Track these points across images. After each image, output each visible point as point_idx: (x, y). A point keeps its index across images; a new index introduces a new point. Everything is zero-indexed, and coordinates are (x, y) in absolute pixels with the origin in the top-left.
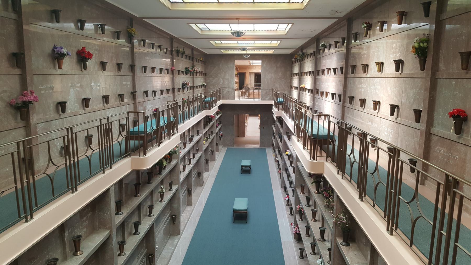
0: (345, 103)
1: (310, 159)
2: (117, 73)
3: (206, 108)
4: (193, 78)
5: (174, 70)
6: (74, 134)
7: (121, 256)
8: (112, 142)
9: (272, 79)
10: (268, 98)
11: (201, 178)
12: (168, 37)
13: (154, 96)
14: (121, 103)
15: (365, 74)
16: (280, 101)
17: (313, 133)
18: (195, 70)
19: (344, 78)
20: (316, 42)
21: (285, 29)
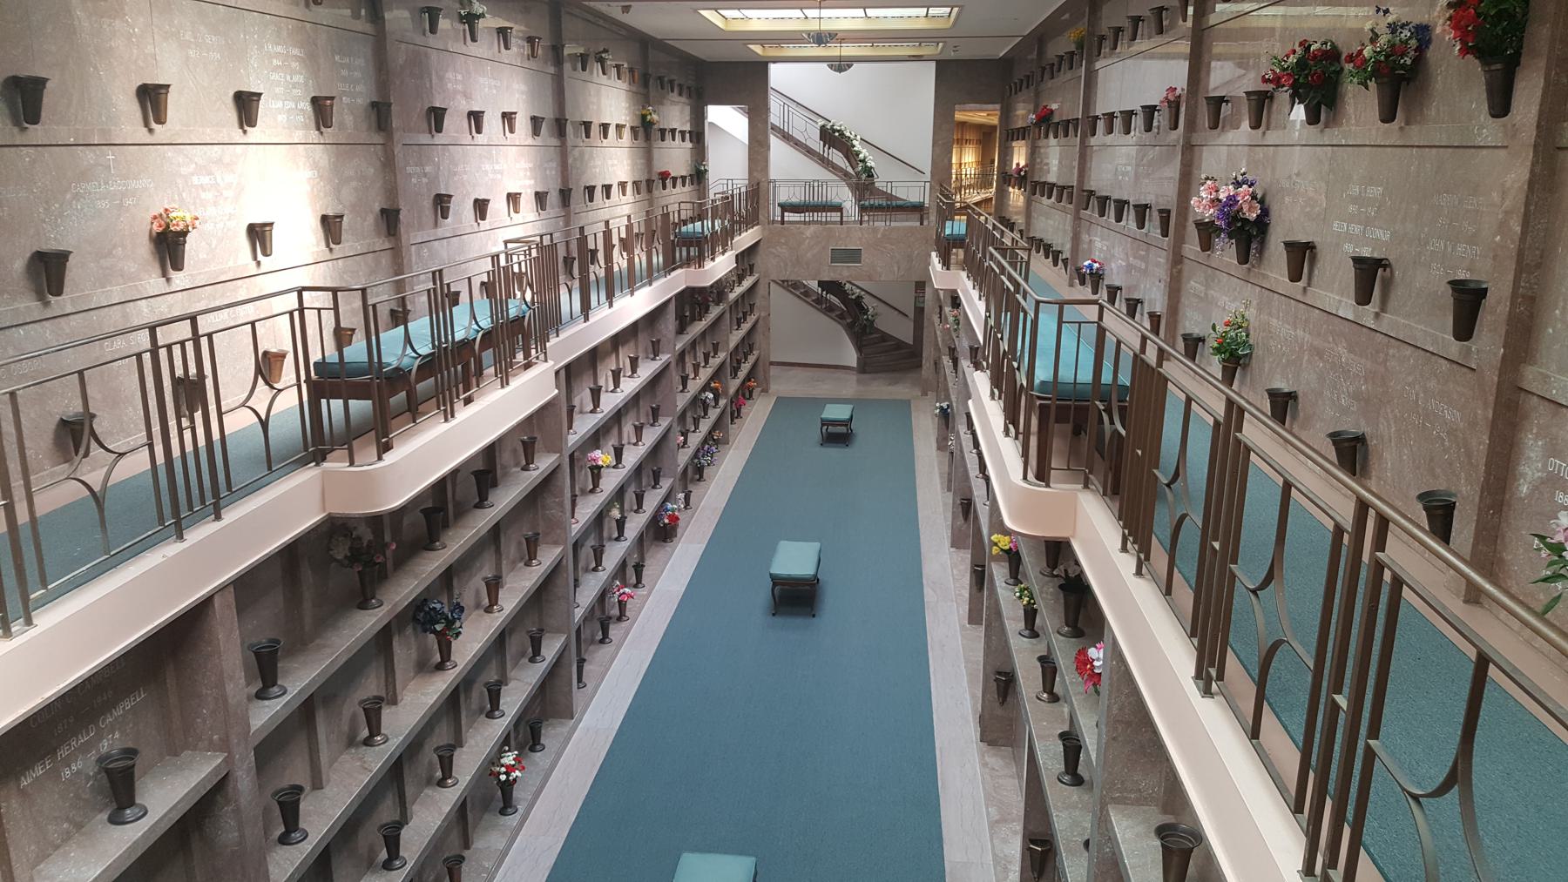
1: (1021, 477)
2: (314, 135)
3: (687, 263)
7: (493, 718)
8: (220, 414)
20: (1087, 14)
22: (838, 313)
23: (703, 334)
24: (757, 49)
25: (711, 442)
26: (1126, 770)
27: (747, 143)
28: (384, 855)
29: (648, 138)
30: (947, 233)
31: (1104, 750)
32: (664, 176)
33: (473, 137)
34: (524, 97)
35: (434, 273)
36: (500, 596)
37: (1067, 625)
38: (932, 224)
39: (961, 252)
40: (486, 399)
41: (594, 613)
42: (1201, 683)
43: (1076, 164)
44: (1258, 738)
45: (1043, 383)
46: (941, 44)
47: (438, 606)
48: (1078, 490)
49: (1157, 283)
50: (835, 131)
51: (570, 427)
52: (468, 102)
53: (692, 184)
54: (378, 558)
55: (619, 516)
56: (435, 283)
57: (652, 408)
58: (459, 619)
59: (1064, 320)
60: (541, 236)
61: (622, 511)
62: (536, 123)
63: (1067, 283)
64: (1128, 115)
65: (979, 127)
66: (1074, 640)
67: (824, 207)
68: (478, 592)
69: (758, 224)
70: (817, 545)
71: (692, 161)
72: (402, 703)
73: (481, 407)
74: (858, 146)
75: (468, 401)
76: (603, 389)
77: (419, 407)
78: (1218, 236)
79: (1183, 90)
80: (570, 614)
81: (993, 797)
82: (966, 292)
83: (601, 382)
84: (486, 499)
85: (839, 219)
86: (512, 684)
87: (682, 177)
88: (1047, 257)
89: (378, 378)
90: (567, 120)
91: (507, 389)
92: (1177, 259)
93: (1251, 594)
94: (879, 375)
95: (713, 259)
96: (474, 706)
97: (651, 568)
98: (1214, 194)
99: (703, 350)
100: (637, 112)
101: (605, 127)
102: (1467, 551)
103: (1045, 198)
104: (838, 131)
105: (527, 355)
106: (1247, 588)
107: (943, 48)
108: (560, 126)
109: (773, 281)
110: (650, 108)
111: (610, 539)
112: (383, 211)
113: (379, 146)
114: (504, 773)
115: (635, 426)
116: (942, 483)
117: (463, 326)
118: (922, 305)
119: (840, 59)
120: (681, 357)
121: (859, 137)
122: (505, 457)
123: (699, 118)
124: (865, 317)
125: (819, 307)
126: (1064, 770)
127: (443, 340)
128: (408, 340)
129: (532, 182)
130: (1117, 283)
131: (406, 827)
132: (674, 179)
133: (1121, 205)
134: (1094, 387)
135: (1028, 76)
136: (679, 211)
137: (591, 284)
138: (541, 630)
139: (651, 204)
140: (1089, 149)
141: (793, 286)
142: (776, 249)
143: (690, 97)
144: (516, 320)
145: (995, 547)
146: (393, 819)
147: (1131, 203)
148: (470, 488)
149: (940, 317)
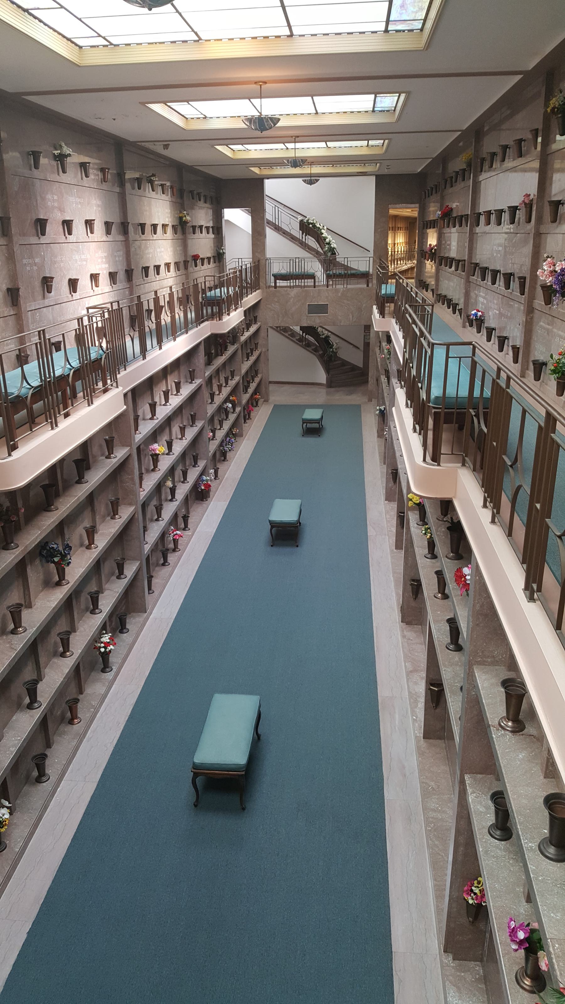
1: (422, 459)
3: (212, 317)
13: (73, 292)
17: (485, 395)
22: (313, 347)
23: (224, 365)
24: (256, 170)
25: (231, 436)
26: (485, 644)
27: (250, 232)
28: (27, 700)
29: (184, 232)
30: (383, 293)
31: (472, 631)
32: (195, 258)
33: (66, 237)
34: (100, 209)
35: (39, 332)
36: (95, 538)
37: (452, 552)
38: (375, 286)
39: (392, 305)
40: (78, 414)
41: (158, 546)
42: (528, 592)
43: (467, 245)
44: (560, 629)
45: (437, 398)
46: (378, 164)
47: (55, 546)
48: (458, 467)
49: (518, 325)
50: (309, 224)
51: (136, 429)
52: (62, 214)
53: (215, 263)
54: (13, 518)
55: (171, 486)
56: (40, 339)
57: (191, 415)
58: (69, 554)
59: (450, 356)
60: (112, 303)
61: (173, 482)
62: (108, 226)
63: (461, 325)
64: (500, 212)
65: (406, 219)
66: (456, 561)
67: (303, 276)
68: (81, 537)
69: (259, 289)
70: (298, 502)
71: (214, 247)
72: (35, 607)
73: (75, 419)
74: (325, 234)
75: (67, 415)
76: (158, 403)
77: (36, 420)
78: (555, 296)
79: (534, 195)
80: (141, 548)
81: (409, 657)
82: (394, 333)
83: (157, 399)
84: (83, 478)
85: (313, 284)
86: (106, 593)
87: (207, 258)
88: (449, 308)
89: (5, 403)
90: (129, 223)
91: (92, 407)
92: (530, 310)
93: (557, 538)
94: (341, 389)
95: (229, 314)
96: (83, 606)
97: (194, 518)
98: (552, 267)
99: (224, 375)
100: (176, 216)
101: (155, 226)
103: (447, 268)
104: (312, 224)
105: (105, 384)
106: (555, 534)
107: (380, 166)
108: (124, 227)
109: (271, 327)
110: (185, 212)
111: (166, 500)
112: (8, 290)
113: (4, 247)
114: (103, 647)
115: (180, 427)
116: (380, 459)
117: (61, 366)
118: (368, 341)
119: (311, 175)
120: (209, 381)
121: (325, 228)
122: (95, 450)
123: (218, 217)
124: (331, 350)
125: (301, 344)
126: (450, 641)
127: (48, 376)
128: (24, 377)
129: (107, 266)
130: (493, 326)
131: (40, 682)
132: (203, 260)
133: (495, 273)
134: (469, 399)
135: (436, 186)
136: (205, 282)
137: (146, 334)
138: (123, 559)
139: (187, 278)
140: (475, 235)
141: (284, 331)
142: (271, 305)
143: (212, 203)
144: (97, 360)
145: (410, 502)
146: (33, 678)
147: (502, 272)
148: (71, 470)
149: (380, 349)
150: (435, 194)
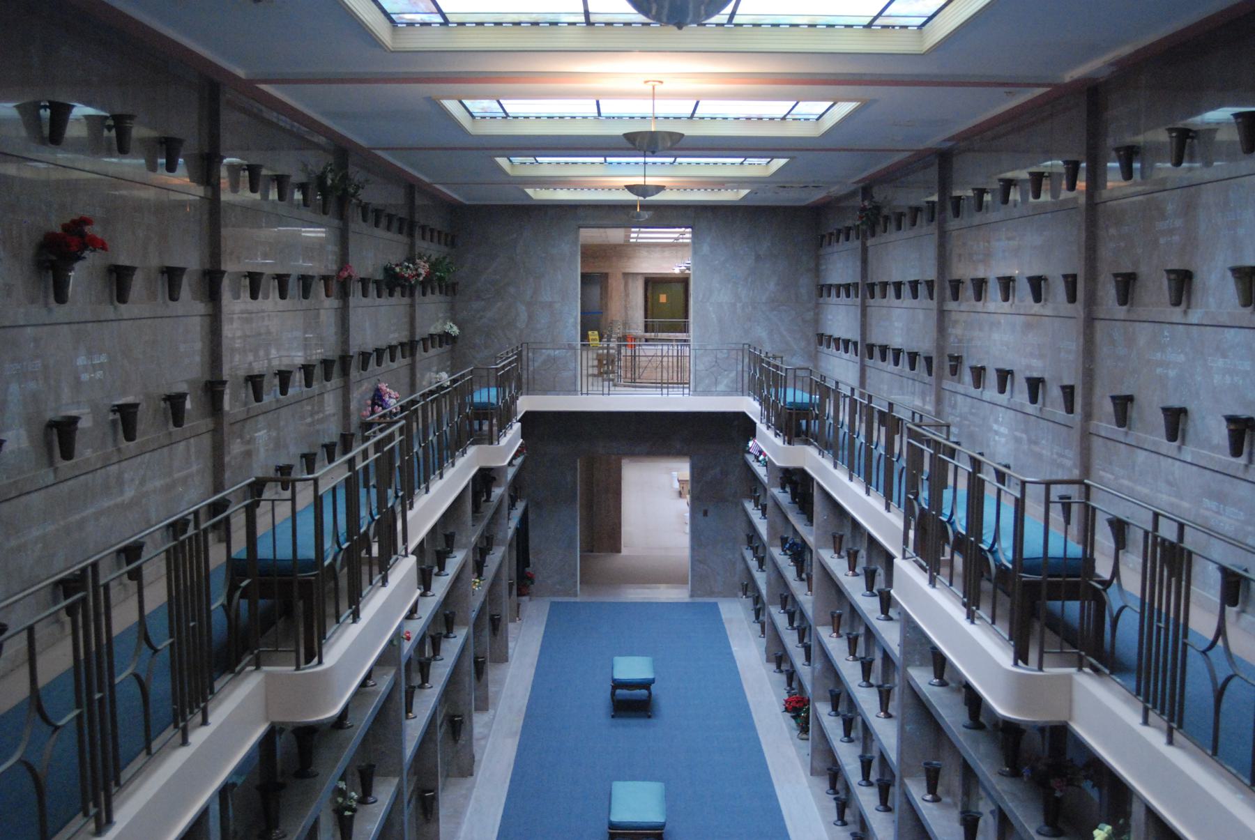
0: (1090, 420)
4: (412, 306)
5: (350, 276)
6: (102, 590)
9: (739, 305)
10: (721, 387)
11: (461, 742)
12: (322, 140)
14: (170, 434)
15: (1178, 310)
16: (798, 400)
17: (1027, 553)
18: (419, 275)
19: (1085, 318)
21: (816, 117)
102: (950, 464)
133: (897, 353)
150: (430, 295)
